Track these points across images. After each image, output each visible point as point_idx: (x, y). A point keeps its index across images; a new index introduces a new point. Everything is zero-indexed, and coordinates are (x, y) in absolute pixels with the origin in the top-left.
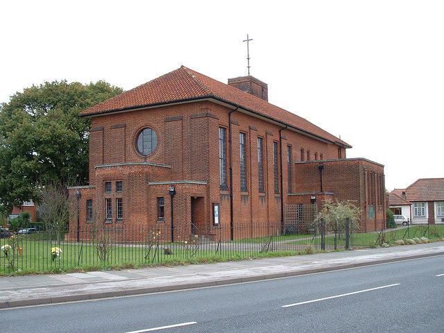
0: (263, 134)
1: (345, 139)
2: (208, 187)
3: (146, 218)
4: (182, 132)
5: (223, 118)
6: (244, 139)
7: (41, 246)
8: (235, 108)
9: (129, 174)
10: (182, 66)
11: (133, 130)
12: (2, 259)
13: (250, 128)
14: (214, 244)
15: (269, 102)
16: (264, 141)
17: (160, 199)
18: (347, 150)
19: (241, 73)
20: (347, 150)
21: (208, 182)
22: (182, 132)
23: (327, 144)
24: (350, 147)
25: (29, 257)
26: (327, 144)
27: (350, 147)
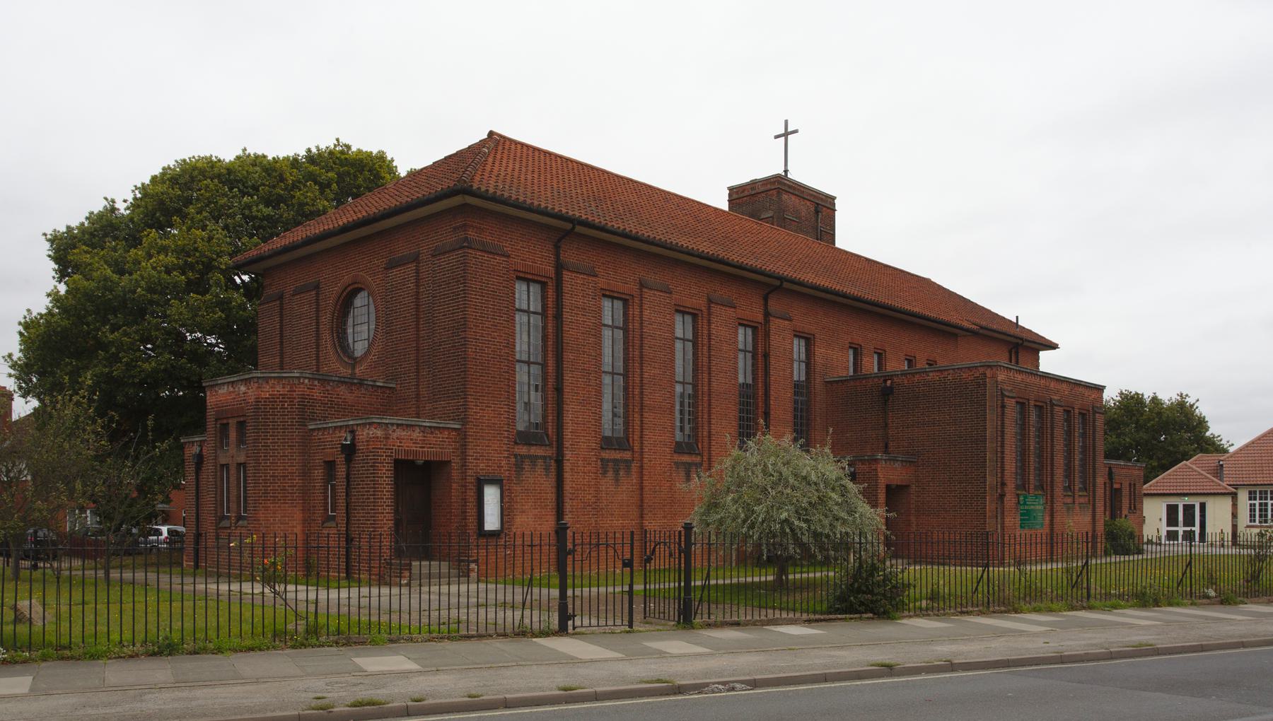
0: (700, 303)
1: (1034, 322)
2: (462, 435)
3: (298, 515)
4: (417, 293)
5: (539, 258)
6: (625, 314)
7: (76, 561)
8: (569, 226)
9: (258, 401)
10: (491, 134)
11: (332, 292)
12: (10, 586)
13: (642, 285)
14: (463, 588)
15: (840, 243)
16: (761, 334)
17: (330, 465)
18: (1042, 354)
19: (764, 167)
20: (1042, 354)
21: (464, 421)
22: (417, 293)
23: (955, 336)
24: (1053, 346)
25: (176, 596)
26: (955, 336)
27: (1053, 346)
